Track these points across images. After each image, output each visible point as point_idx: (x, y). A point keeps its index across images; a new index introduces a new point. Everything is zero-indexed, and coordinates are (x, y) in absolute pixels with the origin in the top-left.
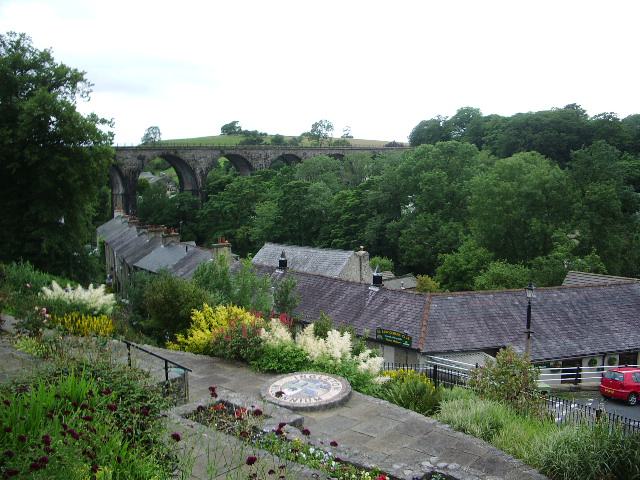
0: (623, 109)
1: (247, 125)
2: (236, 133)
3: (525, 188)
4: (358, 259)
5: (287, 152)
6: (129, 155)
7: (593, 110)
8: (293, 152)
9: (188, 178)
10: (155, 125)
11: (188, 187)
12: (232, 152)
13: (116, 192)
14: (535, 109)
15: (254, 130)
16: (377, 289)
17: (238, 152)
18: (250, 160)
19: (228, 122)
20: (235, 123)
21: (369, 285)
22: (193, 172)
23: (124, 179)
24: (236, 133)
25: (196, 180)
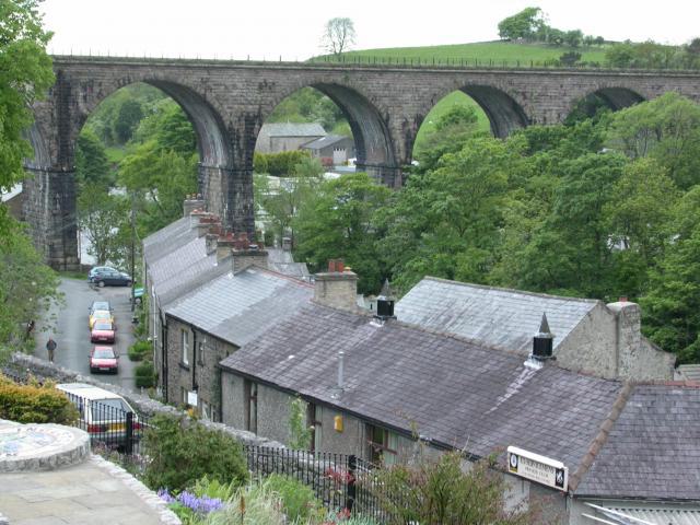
0: (676, 35)
1: (560, 18)
2: (531, 37)
3: (171, 115)
4: (610, 319)
5: (612, 84)
6: (238, 80)
7: (657, 42)
8: (627, 84)
9: (373, 135)
10: (343, 16)
11: (374, 158)
12: (481, 81)
13: (209, 162)
14: (436, 43)
15: (573, 28)
16: (537, 366)
17: (492, 81)
18: (519, 100)
19: (513, 9)
20: (533, 11)
21: (526, 358)
22: (384, 124)
23: (228, 136)
24: (531, 37)
25: (391, 141)
